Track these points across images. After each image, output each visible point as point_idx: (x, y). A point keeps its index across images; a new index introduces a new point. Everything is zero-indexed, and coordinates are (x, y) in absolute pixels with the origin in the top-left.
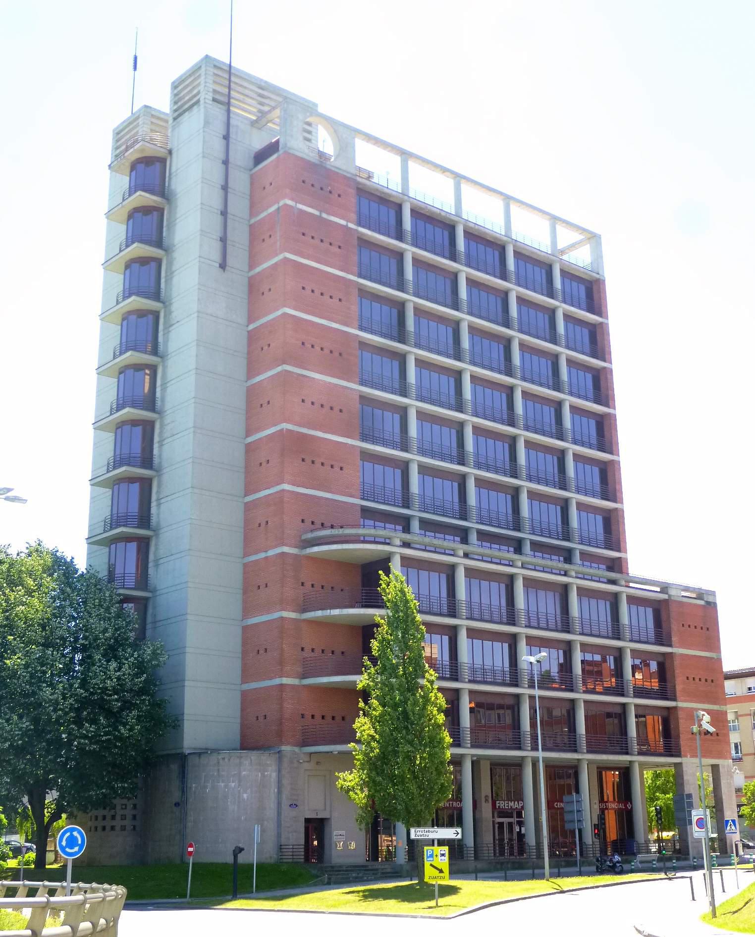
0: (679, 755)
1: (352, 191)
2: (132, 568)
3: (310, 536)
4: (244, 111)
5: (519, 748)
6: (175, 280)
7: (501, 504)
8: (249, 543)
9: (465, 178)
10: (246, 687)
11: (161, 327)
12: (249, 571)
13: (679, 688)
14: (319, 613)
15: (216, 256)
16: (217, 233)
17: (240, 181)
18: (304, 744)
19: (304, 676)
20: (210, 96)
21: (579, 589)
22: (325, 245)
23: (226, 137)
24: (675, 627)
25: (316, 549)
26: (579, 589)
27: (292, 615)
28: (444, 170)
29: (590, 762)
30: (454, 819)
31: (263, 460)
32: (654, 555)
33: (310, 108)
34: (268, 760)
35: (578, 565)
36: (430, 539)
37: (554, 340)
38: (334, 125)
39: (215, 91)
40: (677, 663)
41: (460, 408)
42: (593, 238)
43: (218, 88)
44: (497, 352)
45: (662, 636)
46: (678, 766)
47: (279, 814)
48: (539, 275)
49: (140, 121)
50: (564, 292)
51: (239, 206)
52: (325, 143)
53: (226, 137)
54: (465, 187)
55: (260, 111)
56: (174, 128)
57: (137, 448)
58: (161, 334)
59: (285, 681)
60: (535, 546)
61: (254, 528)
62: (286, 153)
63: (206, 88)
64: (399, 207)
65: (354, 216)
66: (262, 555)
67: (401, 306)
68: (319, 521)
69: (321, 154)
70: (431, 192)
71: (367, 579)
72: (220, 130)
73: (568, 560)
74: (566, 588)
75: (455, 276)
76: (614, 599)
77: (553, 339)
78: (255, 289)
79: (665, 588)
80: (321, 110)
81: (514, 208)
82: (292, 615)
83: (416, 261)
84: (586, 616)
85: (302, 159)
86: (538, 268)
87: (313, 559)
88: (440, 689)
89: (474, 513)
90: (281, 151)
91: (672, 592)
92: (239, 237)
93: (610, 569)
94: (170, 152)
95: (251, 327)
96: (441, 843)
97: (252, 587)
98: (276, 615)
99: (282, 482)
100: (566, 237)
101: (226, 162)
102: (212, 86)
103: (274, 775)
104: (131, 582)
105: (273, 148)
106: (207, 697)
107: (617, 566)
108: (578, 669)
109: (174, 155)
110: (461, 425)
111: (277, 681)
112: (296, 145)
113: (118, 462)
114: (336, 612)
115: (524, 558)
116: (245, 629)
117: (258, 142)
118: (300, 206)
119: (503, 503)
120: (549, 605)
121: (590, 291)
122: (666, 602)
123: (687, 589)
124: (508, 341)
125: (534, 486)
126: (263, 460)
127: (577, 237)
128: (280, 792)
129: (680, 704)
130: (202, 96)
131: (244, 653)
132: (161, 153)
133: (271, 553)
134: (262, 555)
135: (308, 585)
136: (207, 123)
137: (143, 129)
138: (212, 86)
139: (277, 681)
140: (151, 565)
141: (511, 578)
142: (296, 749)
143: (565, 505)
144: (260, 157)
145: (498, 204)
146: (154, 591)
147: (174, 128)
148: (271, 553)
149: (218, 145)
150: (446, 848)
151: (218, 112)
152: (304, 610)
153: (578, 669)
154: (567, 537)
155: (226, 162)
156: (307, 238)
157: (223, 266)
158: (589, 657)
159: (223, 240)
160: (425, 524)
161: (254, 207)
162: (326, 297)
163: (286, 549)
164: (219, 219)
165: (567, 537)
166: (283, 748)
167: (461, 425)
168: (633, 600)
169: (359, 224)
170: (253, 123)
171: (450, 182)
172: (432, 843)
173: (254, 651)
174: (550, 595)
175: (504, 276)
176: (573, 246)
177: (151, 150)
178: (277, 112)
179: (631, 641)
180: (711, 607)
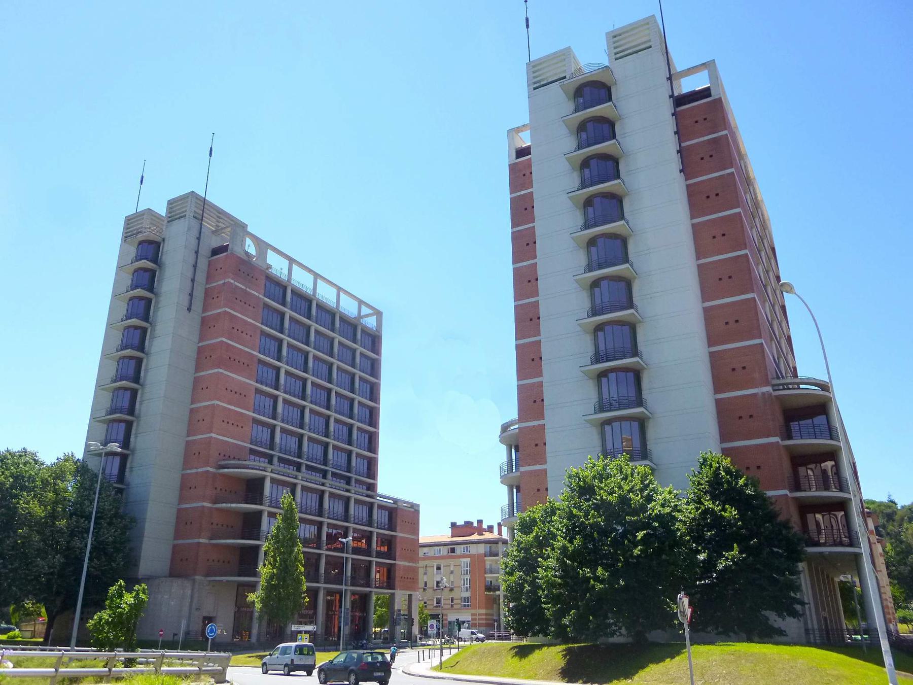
0: (394, 589)
1: (263, 278)
2: (115, 471)
3: (223, 463)
4: (209, 225)
5: (318, 582)
6: (160, 313)
7: (293, 443)
8: (186, 464)
9: (346, 292)
10: (176, 542)
11: (148, 337)
12: (184, 478)
13: (397, 554)
14: (224, 505)
15: (186, 304)
16: (188, 290)
17: (203, 264)
18: (208, 575)
19: (211, 539)
20: (192, 215)
21: (303, 487)
22: (247, 306)
23: (199, 239)
24: (399, 522)
25: (226, 470)
26: (303, 487)
27: (209, 505)
28: (310, 271)
29: (324, 588)
30: (311, 620)
31: (200, 418)
32: (391, 483)
33: (244, 227)
34: (188, 584)
35: (353, 487)
36: (281, 468)
37: (331, 355)
38: (257, 240)
39: (195, 212)
40: (398, 540)
41: (304, 399)
42: (379, 314)
43: (198, 211)
44: (274, 346)
45: (391, 526)
46: (393, 595)
47: (190, 613)
48: (278, 292)
49: (145, 217)
50: (292, 303)
51: (201, 277)
52: (251, 248)
53: (199, 239)
54: (320, 282)
55: (218, 226)
56: (167, 227)
57: (126, 404)
58: (147, 342)
59: (201, 540)
60: (281, 460)
61: (191, 454)
62: (232, 253)
63: (191, 209)
64: (285, 288)
65: (263, 291)
66: (194, 471)
67: (353, 376)
68: (228, 456)
69: (247, 253)
70: (302, 281)
71: (252, 489)
72: (196, 234)
73: (348, 483)
74: (323, 492)
75: (309, 327)
76: (371, 506)
77: (331, 355)
78: (206, 325)
79: (396, 501)
80: (249, 229)
81: (295, 267)
82: (209, 505)
83: (291, 318)
84: (356, 514)
85: (239, 258)
86: (351, 327)
87: (223, 475)
88: (303, 552)
89: (305, 456)
90: (229, 252)
91: (399, 504)
92: (199, 293)
93: (368, 489)
94: (164, 240)
95: (200, 344)
96: (306, 632)
97: (186, 487)
98: (200, 504)
99: (211, 432)
100: (365, 311)
101: (197, 252)
102: (194, 209)
103: (189, 592)
104: (115, 479)
105: (224, 249)
106: (154, 547)
107: (372, 487)
108: (324, 538)
109: (166, 242)
110: (304, 407)
111: (196, 540)
112: (238, 250)
113: (112, 411)
114: (234, 505)
115: (272, 467)
116: (179, 510)
117: (216, 243)
118: (236, 283)
119: (319, 450)
120: (339, 507)
121: (374, 340)
122: (396, 509)
123: (406, 502)
124: (331, 365)
125: (336, 443)
126: (200, 418)
127: (369, 311)
128: (192, 601)
129: (397, 562)
130: (187, 214)
131: (178, 523)
132: (158, 239)
133: (199, 470)
134: (194, 471)
135: (218, 489)
136: (189, 229)
137: (146, 223)
138: (194, 209)
139: (196, 540)
140: (127, 470)
141: (323, 492)
142: (203, 578)
143: (350, 453)
144: (216, 252)
145: (334, 291)
146: (128, 485)
147: (167, 227)
148: (199, 470)
149: (194, 241)
150: (308, 636)
151: (195, 224)
152: (215, 503)
153: (324, 538)
154: (325, 464)
155: (197, 252)
156: (238, 301)
157: (189, 309)
158: (330, 531)
159: (191, 295)
160: (281, 460)
161: (209, 278)
162: (244, 334)
163: (210, 469)
164: (189, 283)
165: (349, 471)
166: (197, 577)
167: (304, 407)
168: (381, 507)
169: (265, 296)
170: (213, 232)
171: (312, 277)
172: (300, 632)
173: (184, 523)
174: (340, 502)
175: (309, 318)
176: (367, 316)
177: (152, 237)
178: (229, 229)
179: (328, 518)
180: (417, 512)
